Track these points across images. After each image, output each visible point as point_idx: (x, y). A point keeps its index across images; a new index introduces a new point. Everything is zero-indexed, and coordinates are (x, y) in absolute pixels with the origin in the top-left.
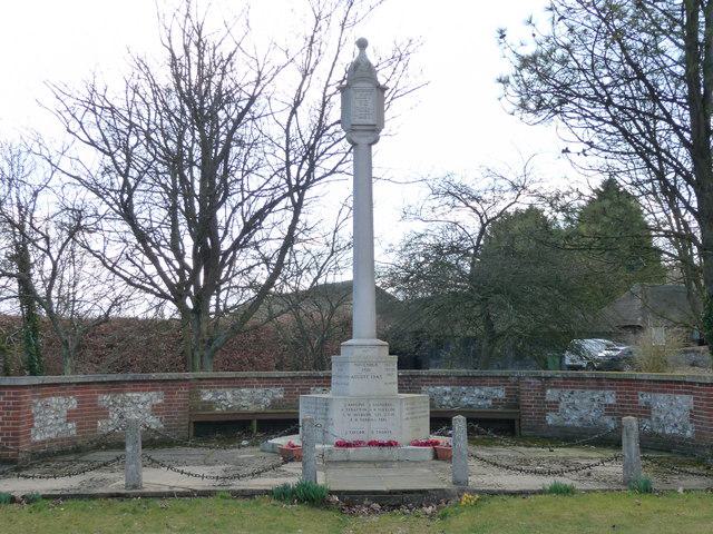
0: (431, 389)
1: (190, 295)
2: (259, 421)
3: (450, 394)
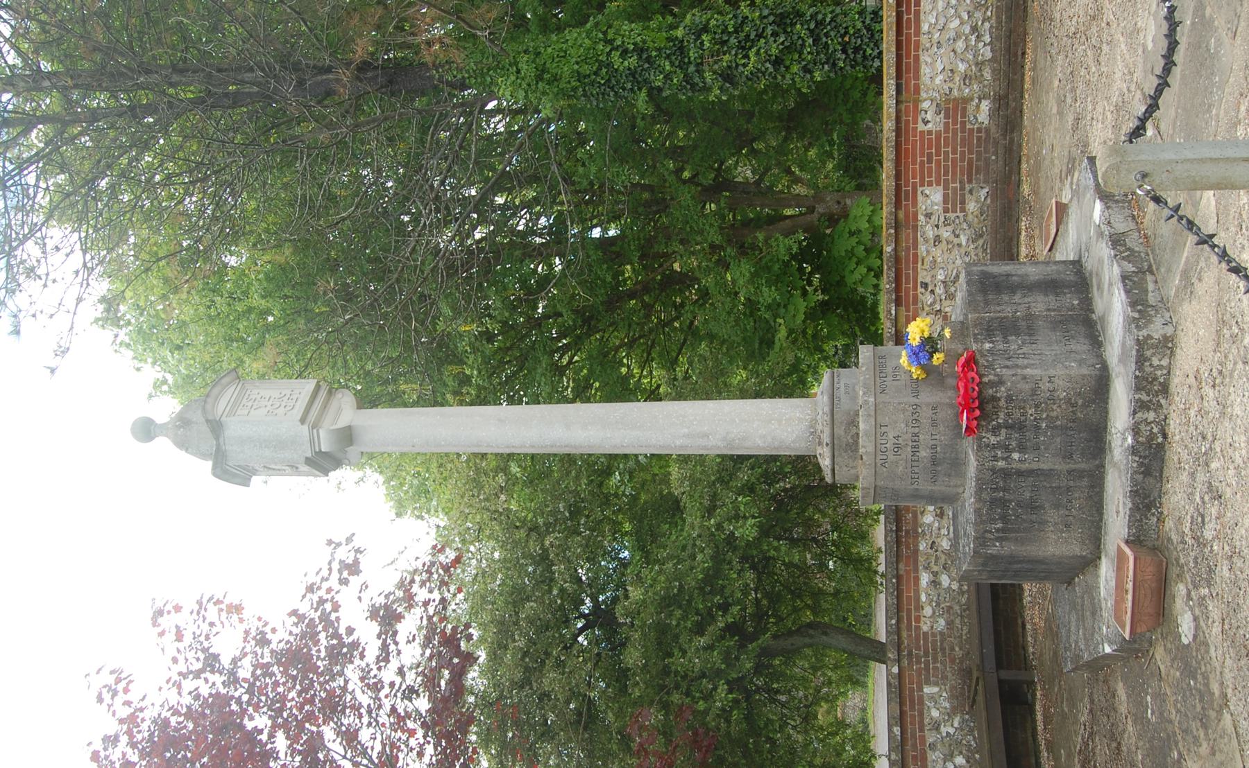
0: (928, 611)
1: (605, 230)
2: (999, 666)
3: (935, 574)
